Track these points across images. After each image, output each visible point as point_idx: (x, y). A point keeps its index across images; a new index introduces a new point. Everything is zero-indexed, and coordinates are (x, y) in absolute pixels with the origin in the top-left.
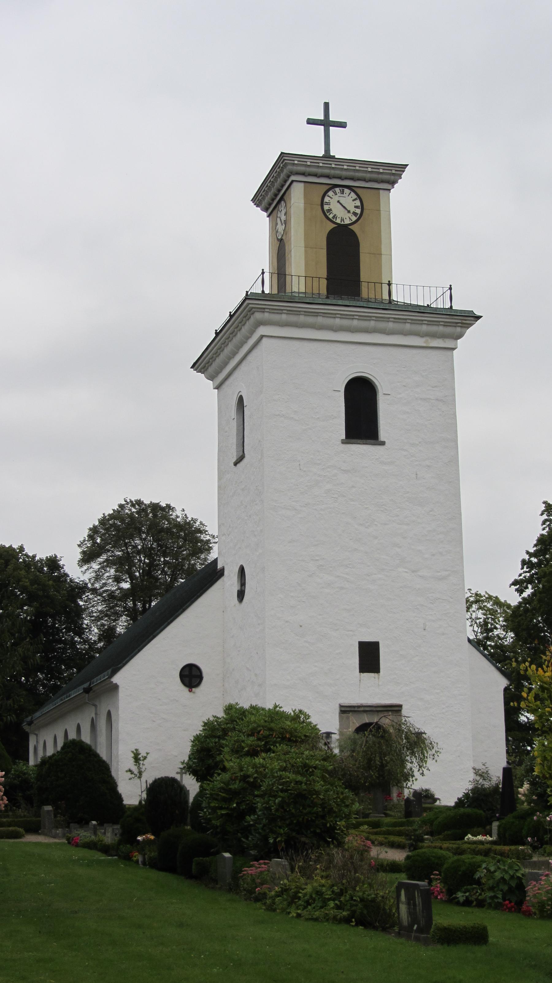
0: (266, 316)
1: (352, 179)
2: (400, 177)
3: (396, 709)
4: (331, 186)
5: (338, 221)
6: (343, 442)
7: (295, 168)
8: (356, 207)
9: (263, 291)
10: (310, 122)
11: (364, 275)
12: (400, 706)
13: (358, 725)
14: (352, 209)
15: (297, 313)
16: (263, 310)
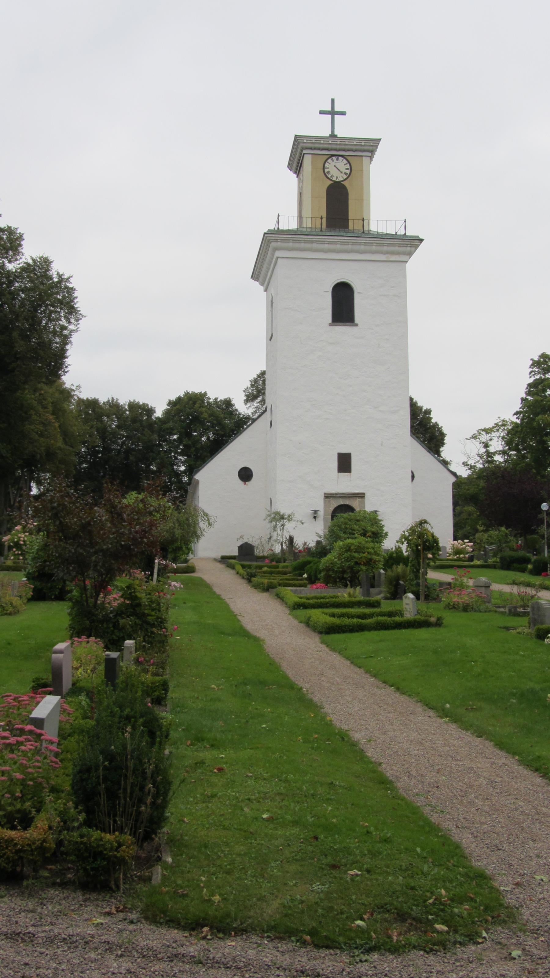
0: (279, 244)
1: (344, 150)
2: (377, 147)
3: (361, 496)
4: (327, 157)
5: (334, 179)
6: (330, 325)
7: (305, 145)
8: (347, 169)
10: (322, 112)
11: (351, 214)
12: (364, 494)
13: (336, 506)
14: (344, 171)
15: (299, 241)
16: (276, 240)
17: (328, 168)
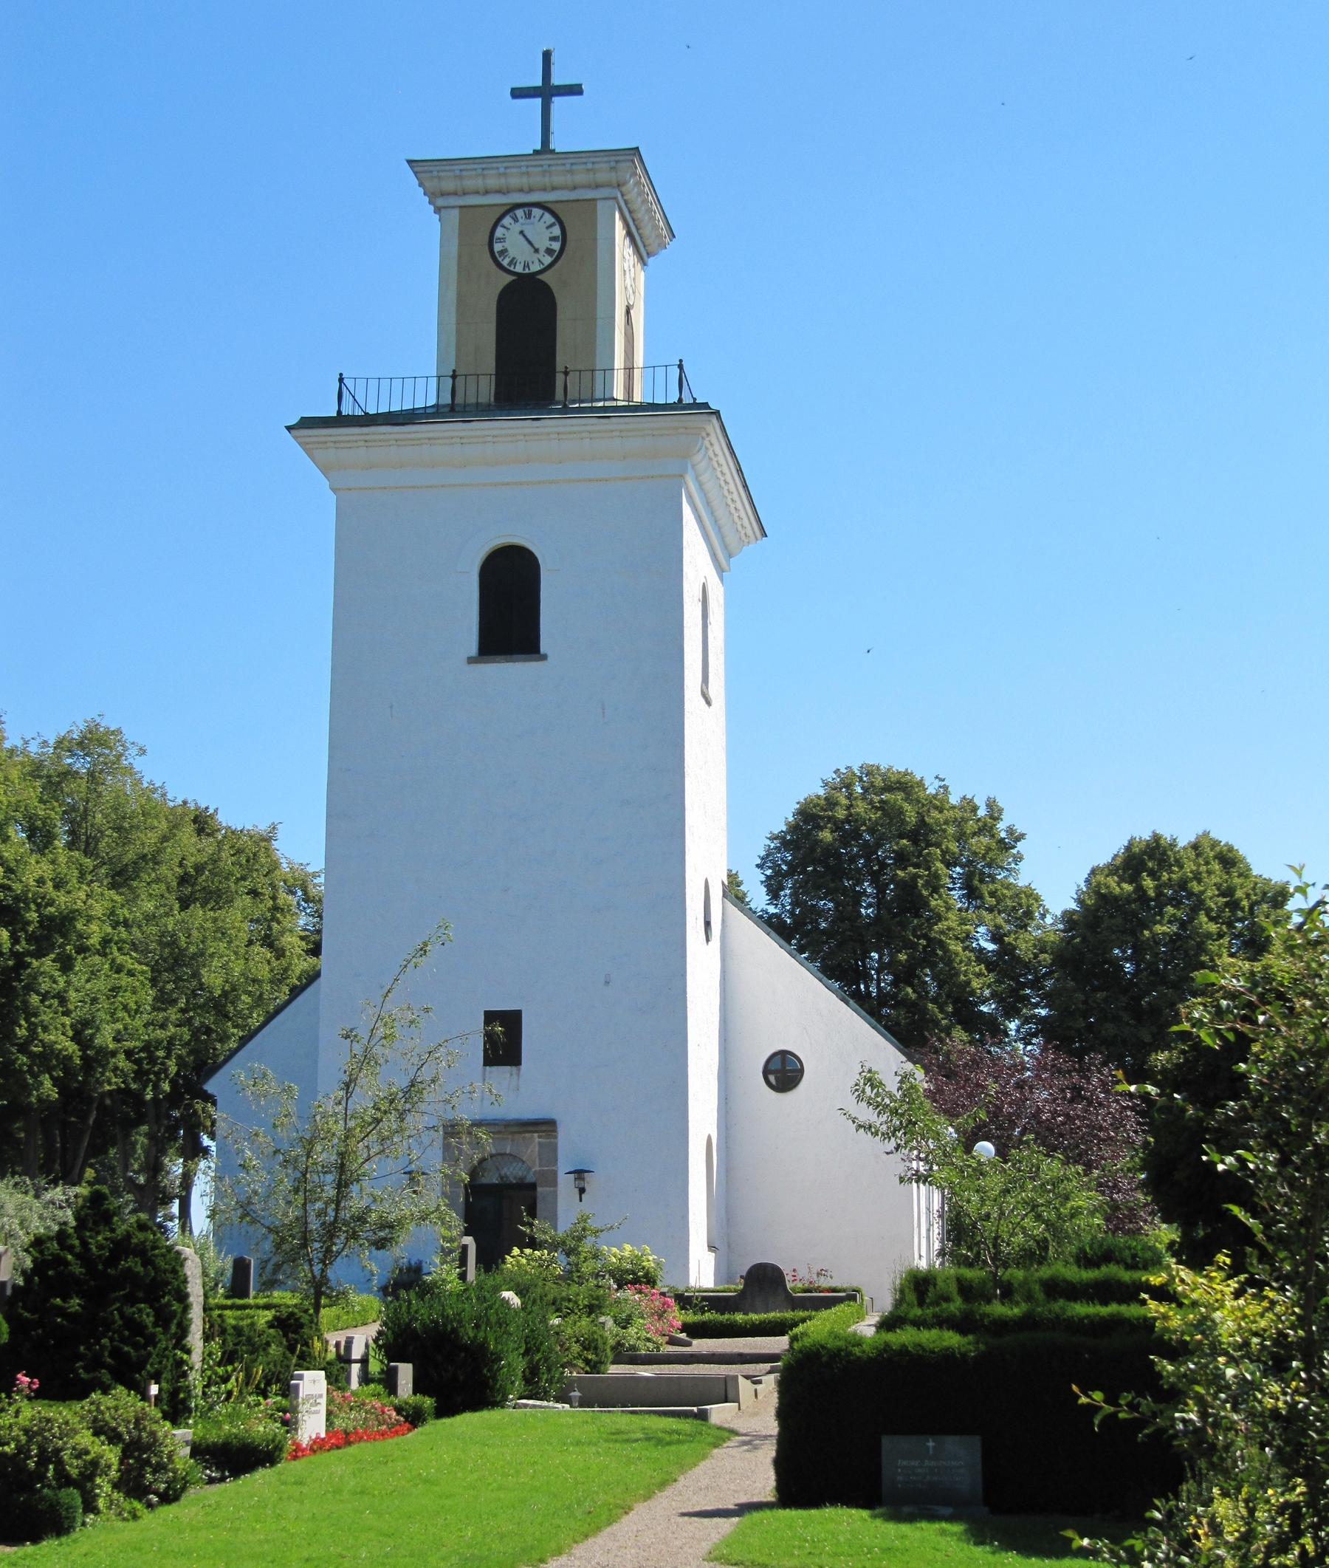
3: (546, 1126)
5: (519, 269)
8: (553, 239)
9: (339, 412)
10: (518, 93)
17: (502, 240)
